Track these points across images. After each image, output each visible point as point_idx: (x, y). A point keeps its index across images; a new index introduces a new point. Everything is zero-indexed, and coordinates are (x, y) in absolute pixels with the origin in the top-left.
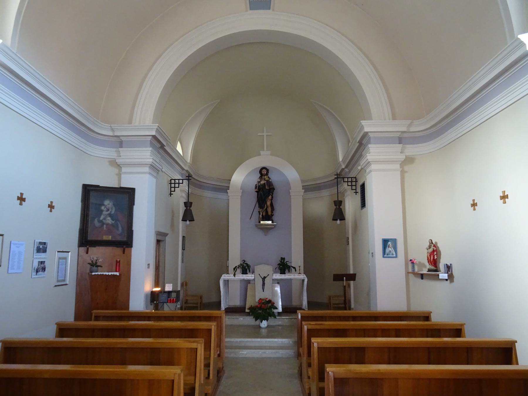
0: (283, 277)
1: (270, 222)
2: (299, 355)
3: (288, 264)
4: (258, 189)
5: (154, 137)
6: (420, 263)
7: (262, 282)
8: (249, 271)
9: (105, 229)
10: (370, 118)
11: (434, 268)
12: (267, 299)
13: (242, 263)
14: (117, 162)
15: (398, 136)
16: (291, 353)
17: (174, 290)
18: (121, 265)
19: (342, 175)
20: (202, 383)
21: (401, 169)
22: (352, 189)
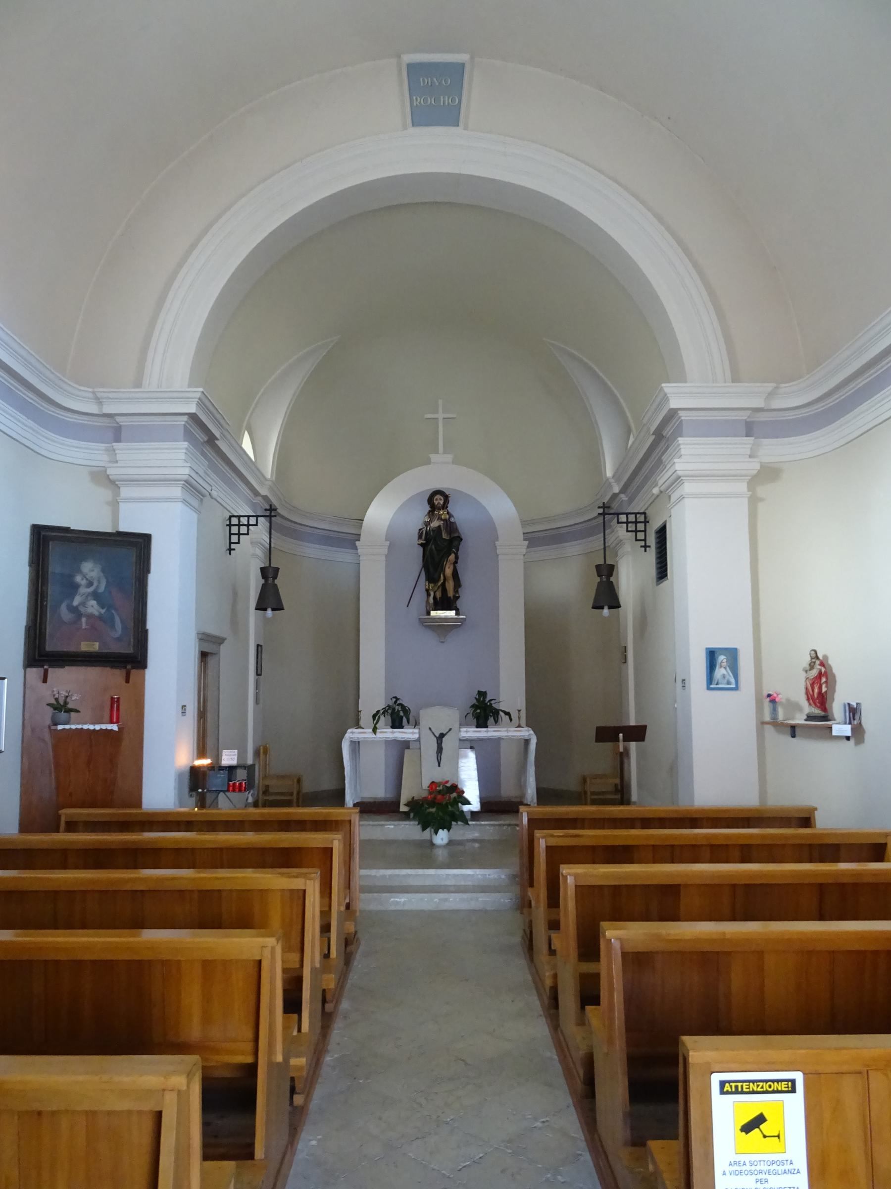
0: (482, 733)
1: (451, 614)
2: (524, 905)
3: (493, 705)
4: (426, 539)
5: (193, 417)
6: (788, 700)
7: (436, 745)
8: (408, 722)
9: (84, 626)
10: (681, 378)
11: (820, 712)
12: (447, 782)
13: (391, 703)
14: (108, 476)
15: (745, 420)
16: (504, 900)
17: (242, 763)
18: (121, 707)
19: (612, 509)
20: (316, 968)
21: (750, 493)
22: (637, 540)
